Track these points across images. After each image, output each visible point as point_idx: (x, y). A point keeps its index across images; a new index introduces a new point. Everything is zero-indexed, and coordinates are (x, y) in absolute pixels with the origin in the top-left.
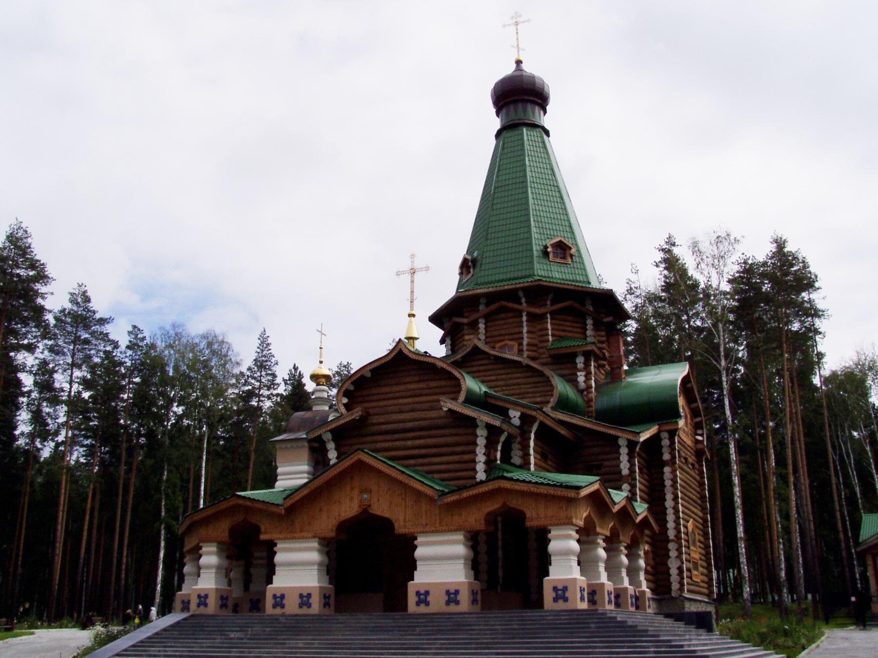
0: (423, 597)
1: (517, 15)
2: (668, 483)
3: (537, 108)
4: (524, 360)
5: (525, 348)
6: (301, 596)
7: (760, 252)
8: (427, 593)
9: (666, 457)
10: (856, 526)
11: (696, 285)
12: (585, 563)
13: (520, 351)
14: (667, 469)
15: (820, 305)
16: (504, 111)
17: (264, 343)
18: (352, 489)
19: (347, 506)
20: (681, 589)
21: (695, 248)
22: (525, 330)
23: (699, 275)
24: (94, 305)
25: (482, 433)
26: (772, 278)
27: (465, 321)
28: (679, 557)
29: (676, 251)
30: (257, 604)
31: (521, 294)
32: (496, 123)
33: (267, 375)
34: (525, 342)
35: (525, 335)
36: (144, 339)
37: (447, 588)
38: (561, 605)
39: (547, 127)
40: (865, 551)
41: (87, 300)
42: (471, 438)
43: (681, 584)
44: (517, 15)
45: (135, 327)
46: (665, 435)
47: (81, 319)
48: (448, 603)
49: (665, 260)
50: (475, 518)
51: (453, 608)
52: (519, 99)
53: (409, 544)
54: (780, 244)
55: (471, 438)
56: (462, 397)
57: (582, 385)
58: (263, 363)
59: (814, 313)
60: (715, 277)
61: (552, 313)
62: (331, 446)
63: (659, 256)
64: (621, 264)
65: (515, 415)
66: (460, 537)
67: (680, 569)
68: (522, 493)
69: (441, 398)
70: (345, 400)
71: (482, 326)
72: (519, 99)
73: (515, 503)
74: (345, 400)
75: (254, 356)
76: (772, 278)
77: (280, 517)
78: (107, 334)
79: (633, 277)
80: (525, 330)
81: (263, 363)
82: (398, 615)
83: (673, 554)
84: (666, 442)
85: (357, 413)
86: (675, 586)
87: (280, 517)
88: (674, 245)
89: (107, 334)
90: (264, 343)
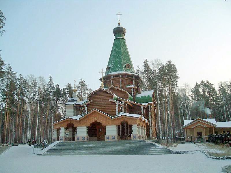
0: (108, 138)
1: (119, 13)
2: (150, 115)
3: (123, 34)
4: (121, 89)
5: (121, 87)
6: (83, 138)
7: (165, 63)
8: (79, 138)
9: (150, 110)
10: (183, 123)
11: (151, 70)
12: (138, 131)
13: (120, 88)
14: (150, 112)
15: (178, 75)
16: (116, 35)
17: (51, 78)
18: (93, 117)
19: (92, 120)
20: (152, 136)
21: (152, 62)
22: (121, 83)
23: (151, 67)
24: (13, 70)
25: (117, 106)
26: (168, 70)
27: (108, 80)
28: (152, 130)
29: (147, 63)
30: (74, 139)
31: (120, 75)
32: (114, 38)
33: (52, 86)
34: (121, 86)
35: (121, 84)
36: (23, 77)
37: (113, 136)
38: (135, 139)
39: (125, 39)
40: (184, 128)
41: (11, 68)
42: (115, 107)
43: (152, 135)
44: (119, 13)
45: (20, 74)
46: (149, 106)
47: (10, 73)
48: (113, 139)
49: (145, 65)
50: (118, 122)
51: (114, 140)
52: (119, 32)
53: (104, 128)
54: (170, 62)
55: (115, 107)
56: (113, 99)
57: (133, 95)
58: (50, 84)
59: (176, 77)
60: (155, 68)
61: (126, 80)
62: (86, 107)
63: (143, 64)
64: (137, 67)
65: (123, 102)
66: (115, 126)
67: (152, 132)
68: (127, 118)
69: (109, 99)
70: (89, 98)
71: (112, 82)
72: (119, 32)
73: (126, 120)
74: (89, 98)
75: (48, 82)
76: (168, 70)
77: (78, 122)
78: (15, 77)
79: (138, 68)
80: (121, 83)
81: (50, 84)
82: (102, 142)
83: (151, 129)
84: (150, 107)
85: (92, 101)
86: (151, 136)
87: (78, 122)
88: (147, 61)
89: (15, 77)
90: (51, 78)
